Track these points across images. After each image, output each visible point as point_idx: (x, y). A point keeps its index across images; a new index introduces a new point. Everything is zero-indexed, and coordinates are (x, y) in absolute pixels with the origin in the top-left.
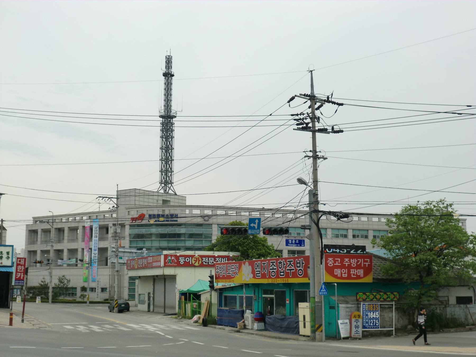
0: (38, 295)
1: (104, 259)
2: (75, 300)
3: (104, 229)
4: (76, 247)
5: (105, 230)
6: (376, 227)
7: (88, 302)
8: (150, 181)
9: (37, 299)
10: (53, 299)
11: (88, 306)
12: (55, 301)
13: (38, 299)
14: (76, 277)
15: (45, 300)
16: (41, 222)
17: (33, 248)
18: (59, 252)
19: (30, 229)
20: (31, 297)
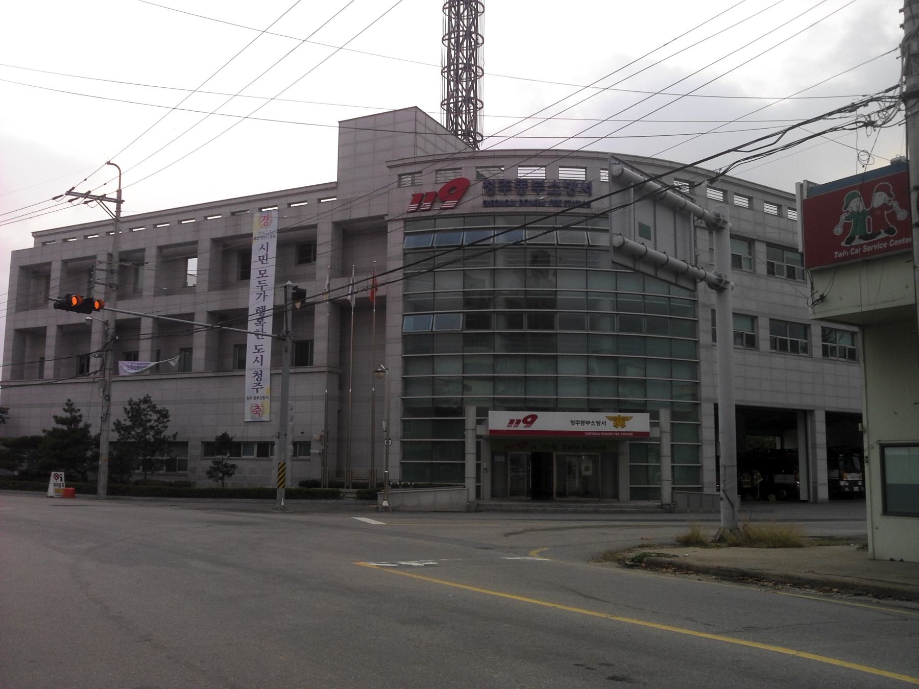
0: (55, 469)
1: (38, 359)
2: (188, 484)
3: (298, 248)
4: (40, 324)
5: (235, 261)
6: (773, 235)
7: (281, 492)
8: (429, 96)
9: (52, 480)
10: (111, 479)
11: (284, 510)
12: (119, 489)
13: (56, 482)
14: (194, 408)
15: (80, 485)
16: (621, 162)
17: (32, 320)
18: (126, 329)
19: (26, 262)
20: (22, 473)
